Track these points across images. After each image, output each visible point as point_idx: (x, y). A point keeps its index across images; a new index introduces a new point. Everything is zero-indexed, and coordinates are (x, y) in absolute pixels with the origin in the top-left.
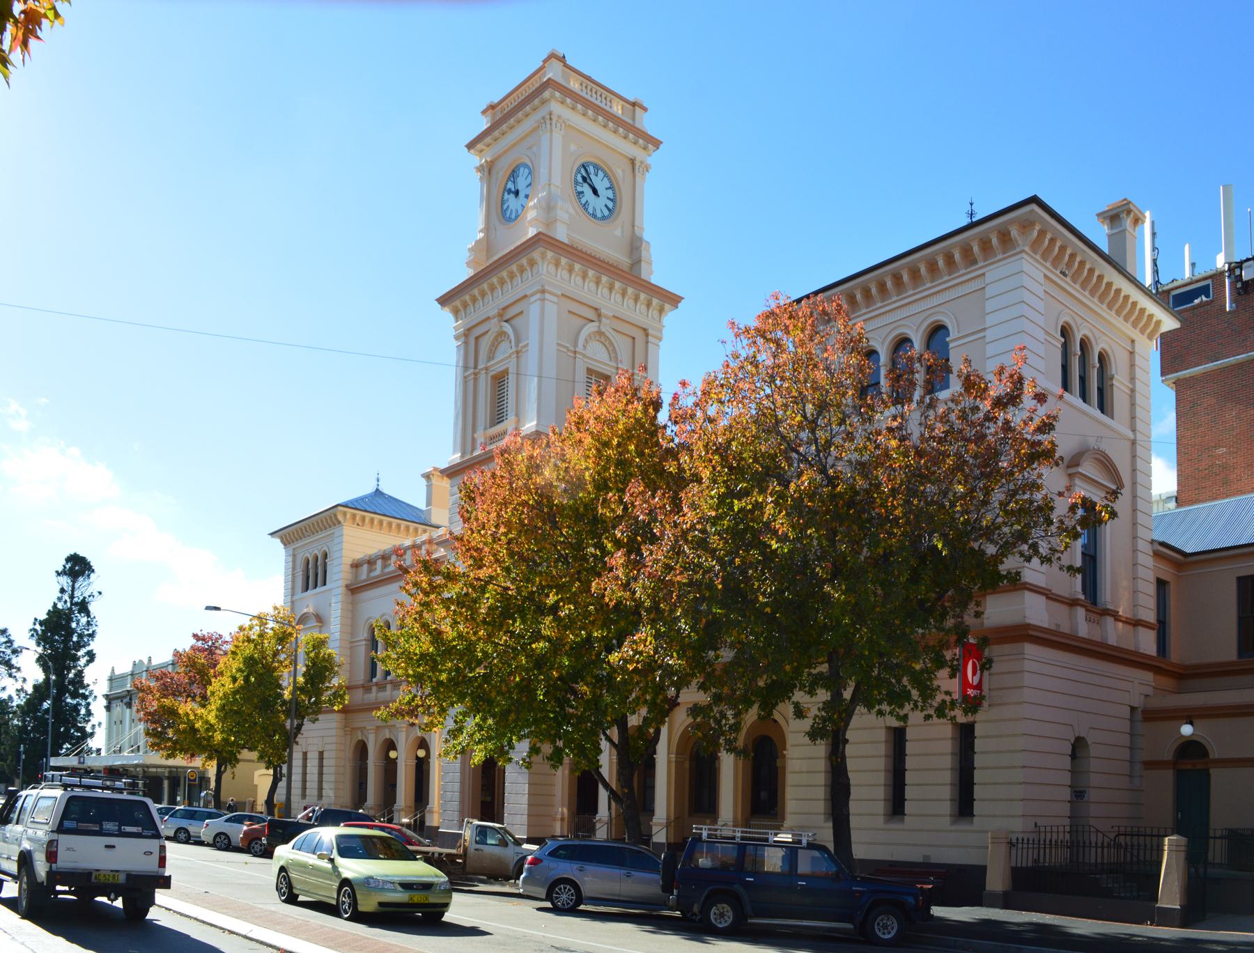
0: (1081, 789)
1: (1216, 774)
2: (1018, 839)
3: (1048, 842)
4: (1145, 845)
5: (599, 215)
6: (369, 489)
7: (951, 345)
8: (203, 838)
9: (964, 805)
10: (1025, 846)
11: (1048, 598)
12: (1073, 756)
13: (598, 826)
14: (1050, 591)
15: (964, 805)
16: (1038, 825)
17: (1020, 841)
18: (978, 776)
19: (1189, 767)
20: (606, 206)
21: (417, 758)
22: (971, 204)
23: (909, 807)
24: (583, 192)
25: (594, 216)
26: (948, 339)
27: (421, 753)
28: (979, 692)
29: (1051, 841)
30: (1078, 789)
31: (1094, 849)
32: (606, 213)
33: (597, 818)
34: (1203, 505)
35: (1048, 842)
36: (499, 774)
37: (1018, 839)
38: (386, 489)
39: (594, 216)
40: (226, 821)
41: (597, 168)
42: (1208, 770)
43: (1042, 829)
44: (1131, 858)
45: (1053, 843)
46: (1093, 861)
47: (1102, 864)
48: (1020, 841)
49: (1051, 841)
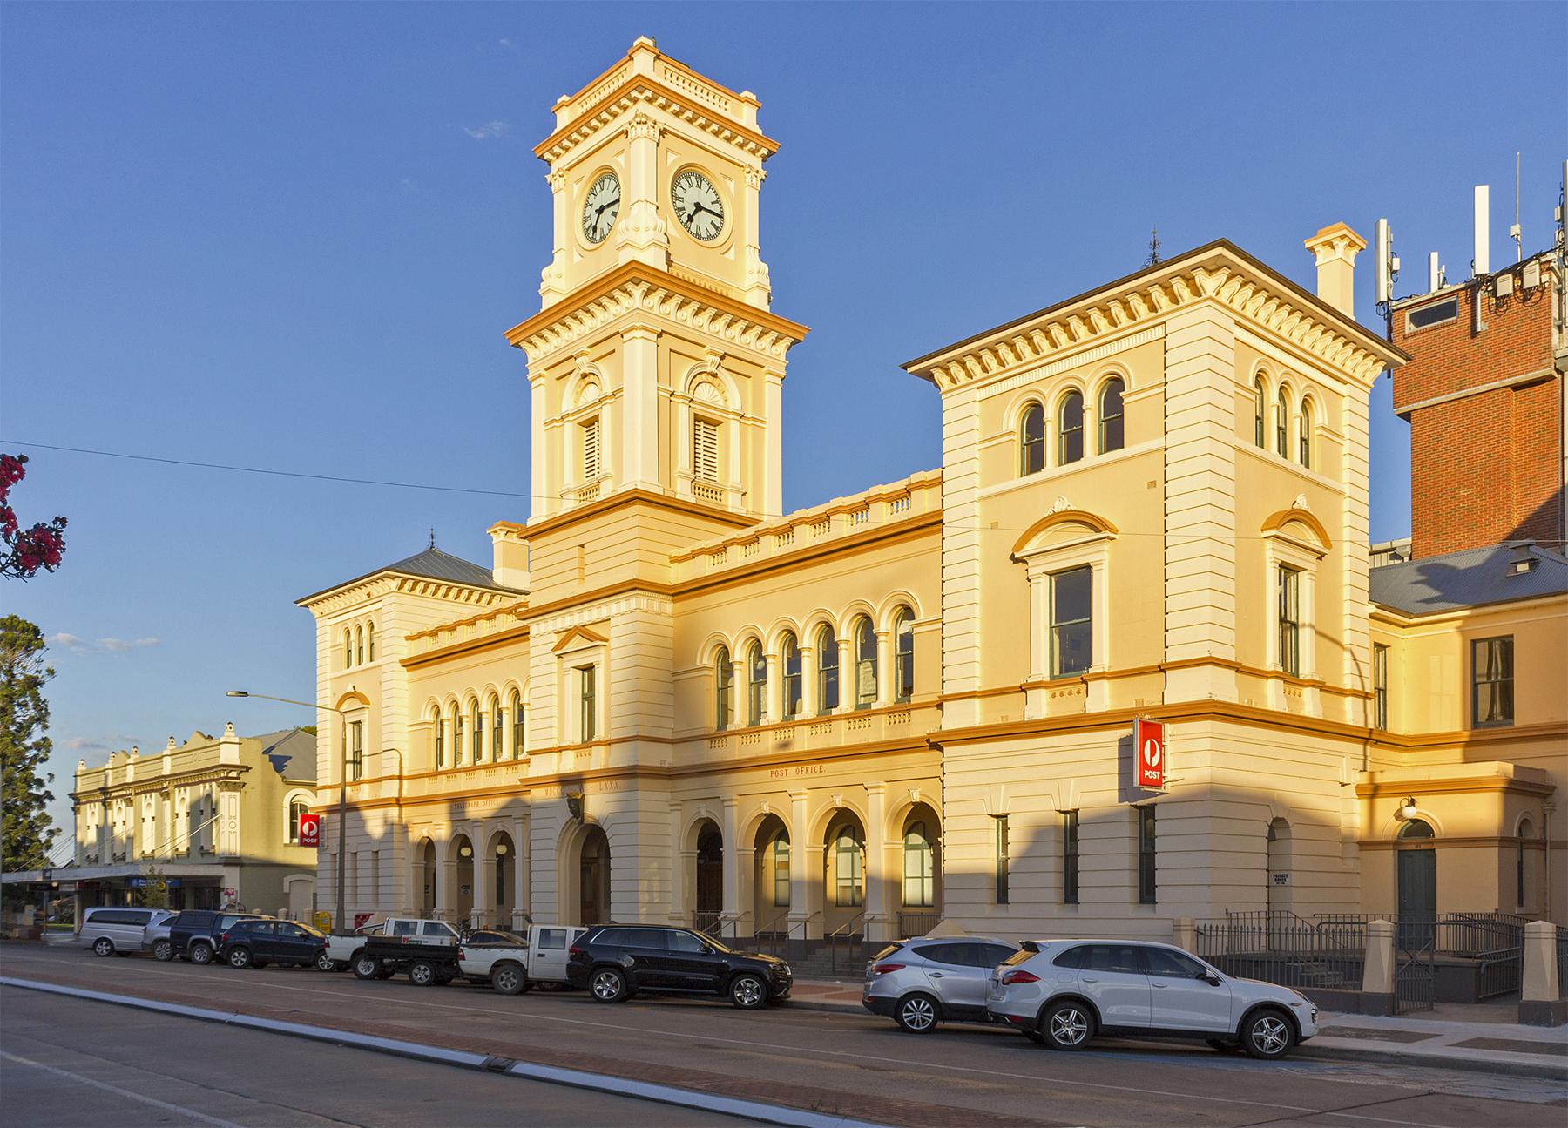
0: (1281, 873)
1: (1441, 854)
2: (1205, 927)
3: (1283, 931)
4: (1260, 928)
5: (704, 235)
6: (422, 547)
7: (1126, 401)
8: (845, 516)
9: (1147, 891)
10: (1214, 933)
11: (1237, 671)
12: (1271, 838)
13: (723, 924)
14: (1240, 664)
15: (1147, 891)
16: (1229, 911)
17: (1208, 928)
18: (1159, 861)
19: (1413, 847)
20: (712, 223)
21: (498, 855)
22: (1155, 233)
23: (1082, 895)
24: (684, 209)
25: (698, 236)
26: (1122, 394)
27: (502, 849)
28: (1158, 773)
29: (1287, 929)
30: (1277, 873)
31: (1221, 938)
32: (713, 231)
33: (722, 916)
34: (118, 968)
35: (1283, 931)
36: (1476, 736)
37: (1205, 927)
38: (443, 547)
39: (698, 236)
40: (757, 522)
41: (679, 210)
42: (1434, 850)
43: (1234, 916)
44: (1334, 946)
45: (1290, 932)
46: (1309, 949)
47: (1312, 951)
48: (1208, 928)
49: (1287, 929)
